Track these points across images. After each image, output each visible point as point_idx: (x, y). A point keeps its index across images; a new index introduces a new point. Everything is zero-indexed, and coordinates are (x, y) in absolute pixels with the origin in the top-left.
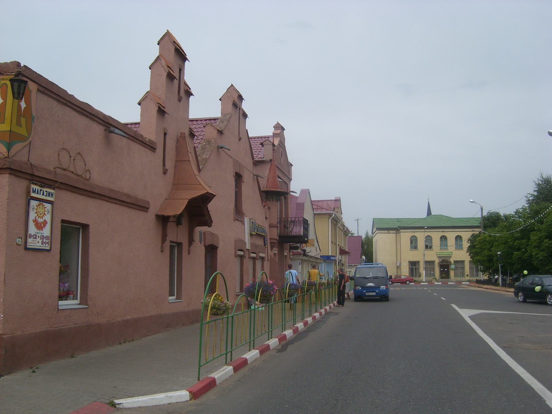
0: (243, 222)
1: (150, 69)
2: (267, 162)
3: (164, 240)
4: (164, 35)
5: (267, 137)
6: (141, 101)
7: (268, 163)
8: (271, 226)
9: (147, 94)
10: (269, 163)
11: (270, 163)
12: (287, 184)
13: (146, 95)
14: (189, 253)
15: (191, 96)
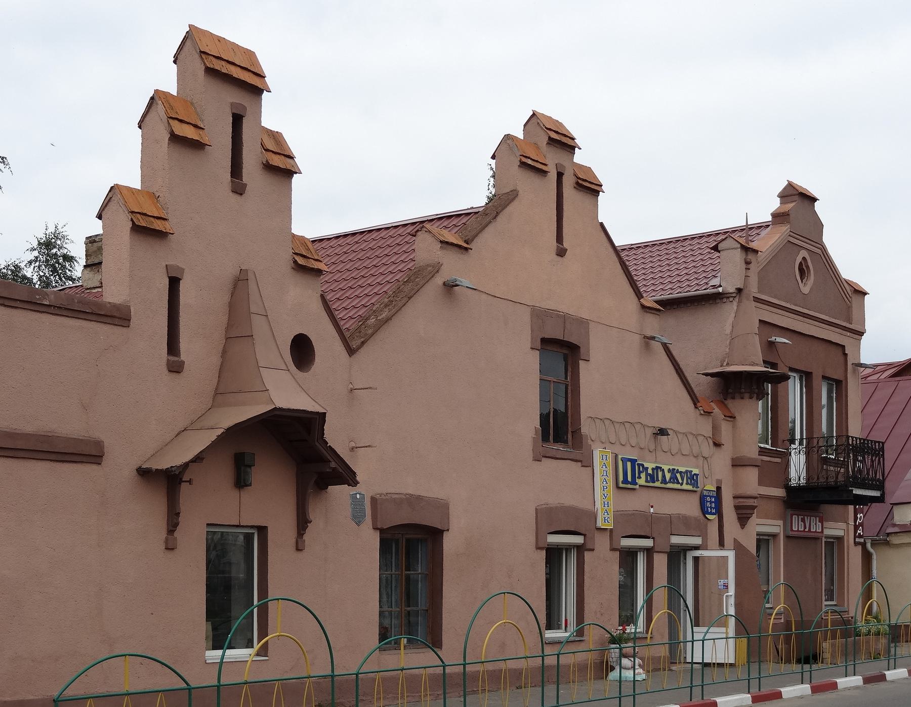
0: (587, 463)
1: (140, 127)
2: (728, 295)
3: (172, 526)
4: (184, 39)
5: (730, 230)
6: (102, 212)
7: (731, 299)
8: (738, 463)
9: (112, 193)
10: (735, 297)
11: (737, 299)
12: (843, 347)
13: (110, 195)
14: (299, 548)
15: (294, 175)
